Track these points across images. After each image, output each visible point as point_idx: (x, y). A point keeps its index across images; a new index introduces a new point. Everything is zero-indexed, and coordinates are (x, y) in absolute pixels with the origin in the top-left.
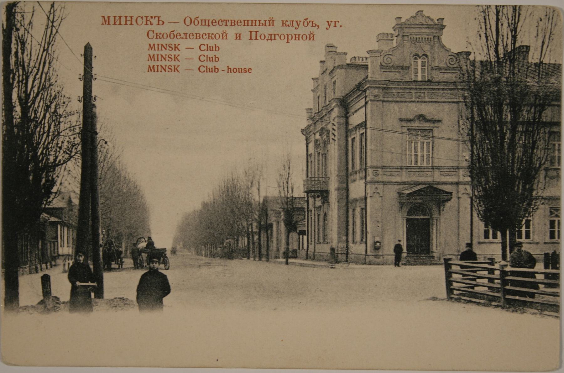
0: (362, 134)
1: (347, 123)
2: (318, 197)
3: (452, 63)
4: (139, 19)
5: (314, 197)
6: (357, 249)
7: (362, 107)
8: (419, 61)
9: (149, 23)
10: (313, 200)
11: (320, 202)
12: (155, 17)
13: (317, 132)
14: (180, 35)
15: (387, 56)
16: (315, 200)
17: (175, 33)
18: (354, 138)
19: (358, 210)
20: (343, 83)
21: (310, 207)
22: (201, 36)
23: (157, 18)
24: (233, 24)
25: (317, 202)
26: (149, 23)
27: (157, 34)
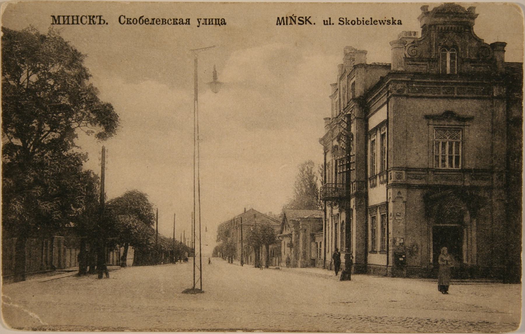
1: (367, 126)
2: (335, 205)
5: (331, 205)
6: (377, 259)
7: (383, 105)
9: (92, 22)
10: (330, 208)
11: (338, 210)
12: (97, 16)
13: (335, 139)
14: (148, 21)
16: (332, 208)
17: (144, 18)
18: (374, 140)
20: (360, 83)
21: (328, 216)
22: (167, 21)
23: (98, 17)
24: (164, 23)
25: (334, 210)
26: (92, 22)
27: (127, 19)
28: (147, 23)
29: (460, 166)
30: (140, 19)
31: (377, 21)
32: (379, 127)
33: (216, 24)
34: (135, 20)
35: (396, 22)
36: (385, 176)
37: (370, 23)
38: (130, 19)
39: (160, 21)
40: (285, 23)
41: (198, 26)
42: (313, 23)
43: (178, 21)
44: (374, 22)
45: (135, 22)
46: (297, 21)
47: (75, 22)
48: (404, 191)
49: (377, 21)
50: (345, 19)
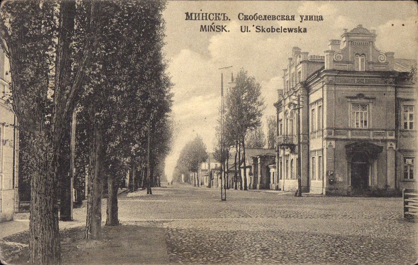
0: (320, 107)
3: (382, 60)
4: (211, 16)
8: (360, 58)
9: (217, 19)
14: (262, 17)
15: (338, 55)
16: (284, 150)
17: (258, 15)
18: (314, 109)
19: (317, 158)
22: (276, 18)
23: (223, 15)
24: (274, 19)
26: (217, 19)
27: (245, 16)
28: (261, 19)
29: (367, 126)
30: (254, 16)
31: (286, 29)
32: (316, 102)
33: (315, 20)
34: (256, 19)
35: (302, 30)
36: (321, 132)
37: (280, 30)
38: (248, 16)
39: (271, 17)
40: (246, 28)
41: (301, 22)
42: (227, 31)
43: (285, 18)
44: (284, 29)
45: (251, 18)
46: (216, 29)
47: (204, 18)
48: (333, 143)
49: (286, 29)
50: (261, 27)
